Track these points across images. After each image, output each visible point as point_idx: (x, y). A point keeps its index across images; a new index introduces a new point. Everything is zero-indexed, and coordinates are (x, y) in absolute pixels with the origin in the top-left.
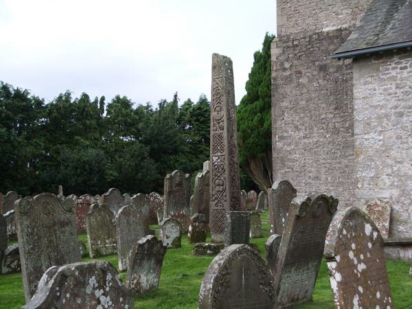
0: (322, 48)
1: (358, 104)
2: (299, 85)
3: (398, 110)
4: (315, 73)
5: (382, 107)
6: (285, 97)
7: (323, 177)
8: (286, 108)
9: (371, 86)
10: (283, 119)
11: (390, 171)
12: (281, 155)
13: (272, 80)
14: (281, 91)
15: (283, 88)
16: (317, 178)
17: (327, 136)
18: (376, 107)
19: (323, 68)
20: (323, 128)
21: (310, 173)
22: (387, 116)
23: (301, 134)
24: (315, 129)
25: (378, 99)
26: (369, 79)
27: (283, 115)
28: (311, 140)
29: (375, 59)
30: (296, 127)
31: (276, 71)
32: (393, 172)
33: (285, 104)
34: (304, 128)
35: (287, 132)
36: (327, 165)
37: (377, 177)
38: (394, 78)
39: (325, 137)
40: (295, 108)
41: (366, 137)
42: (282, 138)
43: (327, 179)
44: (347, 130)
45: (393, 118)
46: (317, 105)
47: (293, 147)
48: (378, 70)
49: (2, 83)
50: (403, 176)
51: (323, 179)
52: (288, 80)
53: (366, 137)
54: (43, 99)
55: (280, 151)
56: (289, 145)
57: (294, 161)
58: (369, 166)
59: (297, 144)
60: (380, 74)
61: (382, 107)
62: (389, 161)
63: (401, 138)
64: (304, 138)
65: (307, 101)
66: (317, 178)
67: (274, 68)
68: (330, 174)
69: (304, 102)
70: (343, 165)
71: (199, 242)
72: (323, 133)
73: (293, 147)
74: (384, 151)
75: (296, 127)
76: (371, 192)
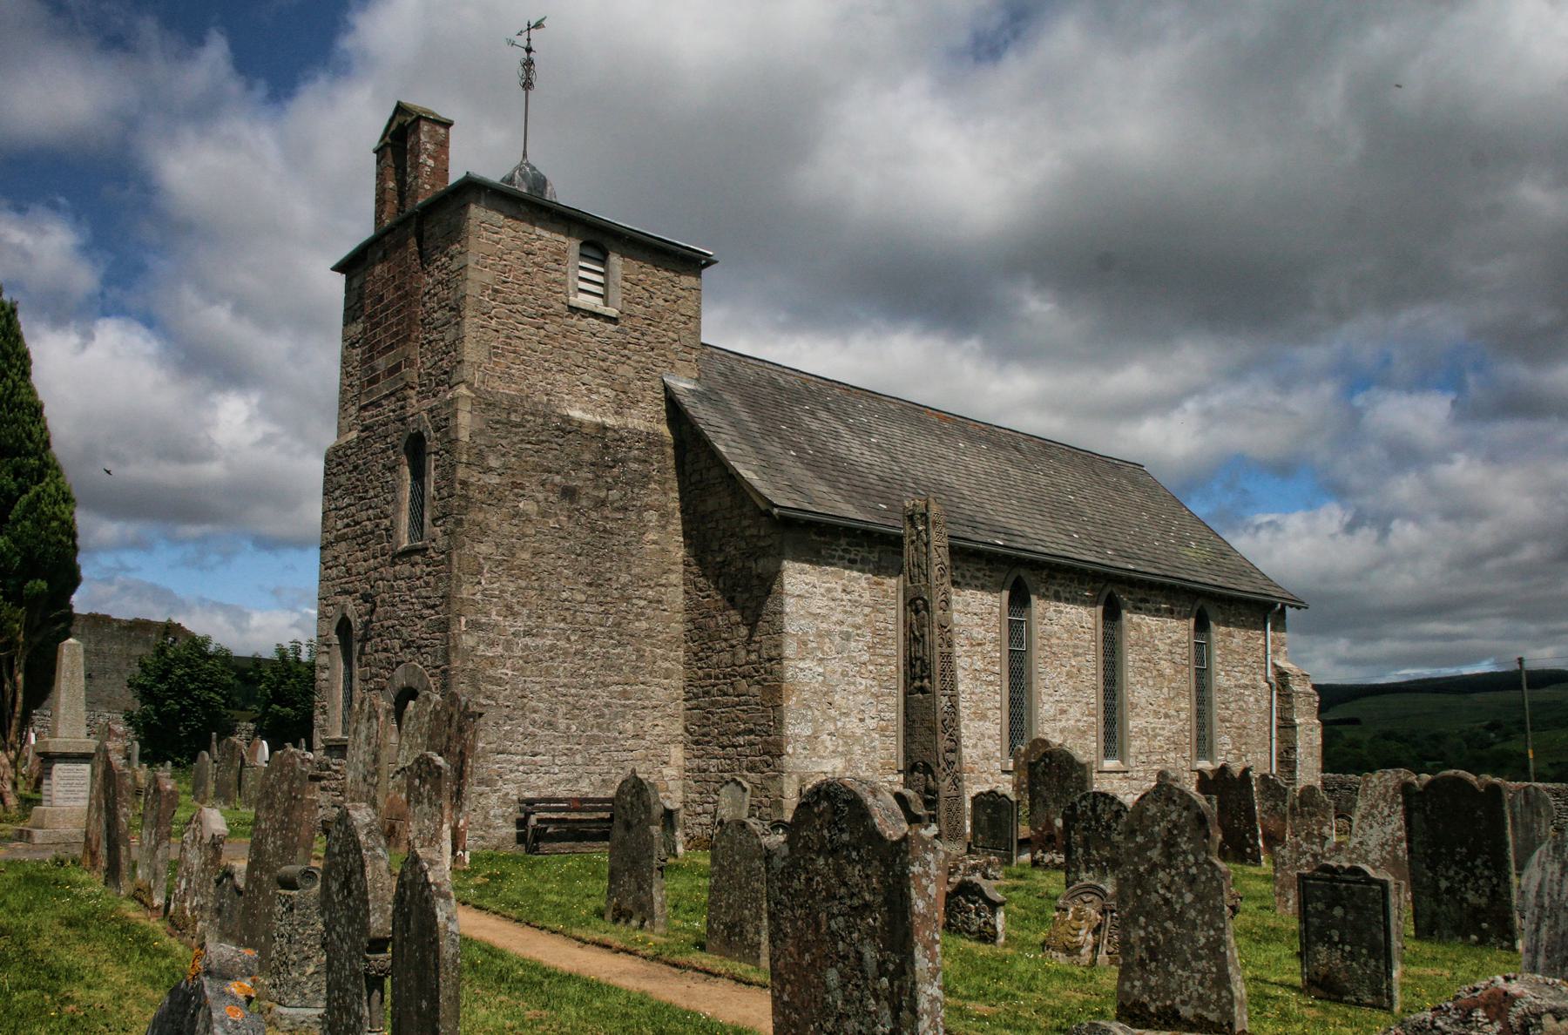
0: (568, 450)
1: (790, 605)
3: (844, 628)
5: (825, 617)
6: (484, 533)
7: (562, 723)
9: (808, 578)
11: (832, 728)
12: (470, 665)
15: (481, 509)
16: (551, 725)
17: (573, 638)
19: (569, 493)
20: (564, 620)
22: (829, 633)
23: (520, 625)
24: (550, 619)
25: (818, 604)
27: (480, 573)
28: (539, 641)
31: (468, 464)
33: (483, 548)
34: (525, 611)
35: (487, 614)
36: (570, 699)
37: (815, 737)
39: (568, 639)
40: (507, 564)
41: (801, 665)
42: (474, 626)
43: (568, 728)
45: (837, 639)
47: (500, 650)
49: (1521, 660)
51: (562, 727)
52: (495, 498)
53: (801, 665)
56: (492, 644)
57: (498, 682)
58: (804, 716)
59: (508, 646)
61: (825, 617)
62: (833, 712)
64: (527, 633)
65: (535, 554)
67: (464, 458)
69: (526, 556)
70: (599, 702)
71: (1496, 774)
73: (500, 650)
74: (826, 694)
75: (509, 608)
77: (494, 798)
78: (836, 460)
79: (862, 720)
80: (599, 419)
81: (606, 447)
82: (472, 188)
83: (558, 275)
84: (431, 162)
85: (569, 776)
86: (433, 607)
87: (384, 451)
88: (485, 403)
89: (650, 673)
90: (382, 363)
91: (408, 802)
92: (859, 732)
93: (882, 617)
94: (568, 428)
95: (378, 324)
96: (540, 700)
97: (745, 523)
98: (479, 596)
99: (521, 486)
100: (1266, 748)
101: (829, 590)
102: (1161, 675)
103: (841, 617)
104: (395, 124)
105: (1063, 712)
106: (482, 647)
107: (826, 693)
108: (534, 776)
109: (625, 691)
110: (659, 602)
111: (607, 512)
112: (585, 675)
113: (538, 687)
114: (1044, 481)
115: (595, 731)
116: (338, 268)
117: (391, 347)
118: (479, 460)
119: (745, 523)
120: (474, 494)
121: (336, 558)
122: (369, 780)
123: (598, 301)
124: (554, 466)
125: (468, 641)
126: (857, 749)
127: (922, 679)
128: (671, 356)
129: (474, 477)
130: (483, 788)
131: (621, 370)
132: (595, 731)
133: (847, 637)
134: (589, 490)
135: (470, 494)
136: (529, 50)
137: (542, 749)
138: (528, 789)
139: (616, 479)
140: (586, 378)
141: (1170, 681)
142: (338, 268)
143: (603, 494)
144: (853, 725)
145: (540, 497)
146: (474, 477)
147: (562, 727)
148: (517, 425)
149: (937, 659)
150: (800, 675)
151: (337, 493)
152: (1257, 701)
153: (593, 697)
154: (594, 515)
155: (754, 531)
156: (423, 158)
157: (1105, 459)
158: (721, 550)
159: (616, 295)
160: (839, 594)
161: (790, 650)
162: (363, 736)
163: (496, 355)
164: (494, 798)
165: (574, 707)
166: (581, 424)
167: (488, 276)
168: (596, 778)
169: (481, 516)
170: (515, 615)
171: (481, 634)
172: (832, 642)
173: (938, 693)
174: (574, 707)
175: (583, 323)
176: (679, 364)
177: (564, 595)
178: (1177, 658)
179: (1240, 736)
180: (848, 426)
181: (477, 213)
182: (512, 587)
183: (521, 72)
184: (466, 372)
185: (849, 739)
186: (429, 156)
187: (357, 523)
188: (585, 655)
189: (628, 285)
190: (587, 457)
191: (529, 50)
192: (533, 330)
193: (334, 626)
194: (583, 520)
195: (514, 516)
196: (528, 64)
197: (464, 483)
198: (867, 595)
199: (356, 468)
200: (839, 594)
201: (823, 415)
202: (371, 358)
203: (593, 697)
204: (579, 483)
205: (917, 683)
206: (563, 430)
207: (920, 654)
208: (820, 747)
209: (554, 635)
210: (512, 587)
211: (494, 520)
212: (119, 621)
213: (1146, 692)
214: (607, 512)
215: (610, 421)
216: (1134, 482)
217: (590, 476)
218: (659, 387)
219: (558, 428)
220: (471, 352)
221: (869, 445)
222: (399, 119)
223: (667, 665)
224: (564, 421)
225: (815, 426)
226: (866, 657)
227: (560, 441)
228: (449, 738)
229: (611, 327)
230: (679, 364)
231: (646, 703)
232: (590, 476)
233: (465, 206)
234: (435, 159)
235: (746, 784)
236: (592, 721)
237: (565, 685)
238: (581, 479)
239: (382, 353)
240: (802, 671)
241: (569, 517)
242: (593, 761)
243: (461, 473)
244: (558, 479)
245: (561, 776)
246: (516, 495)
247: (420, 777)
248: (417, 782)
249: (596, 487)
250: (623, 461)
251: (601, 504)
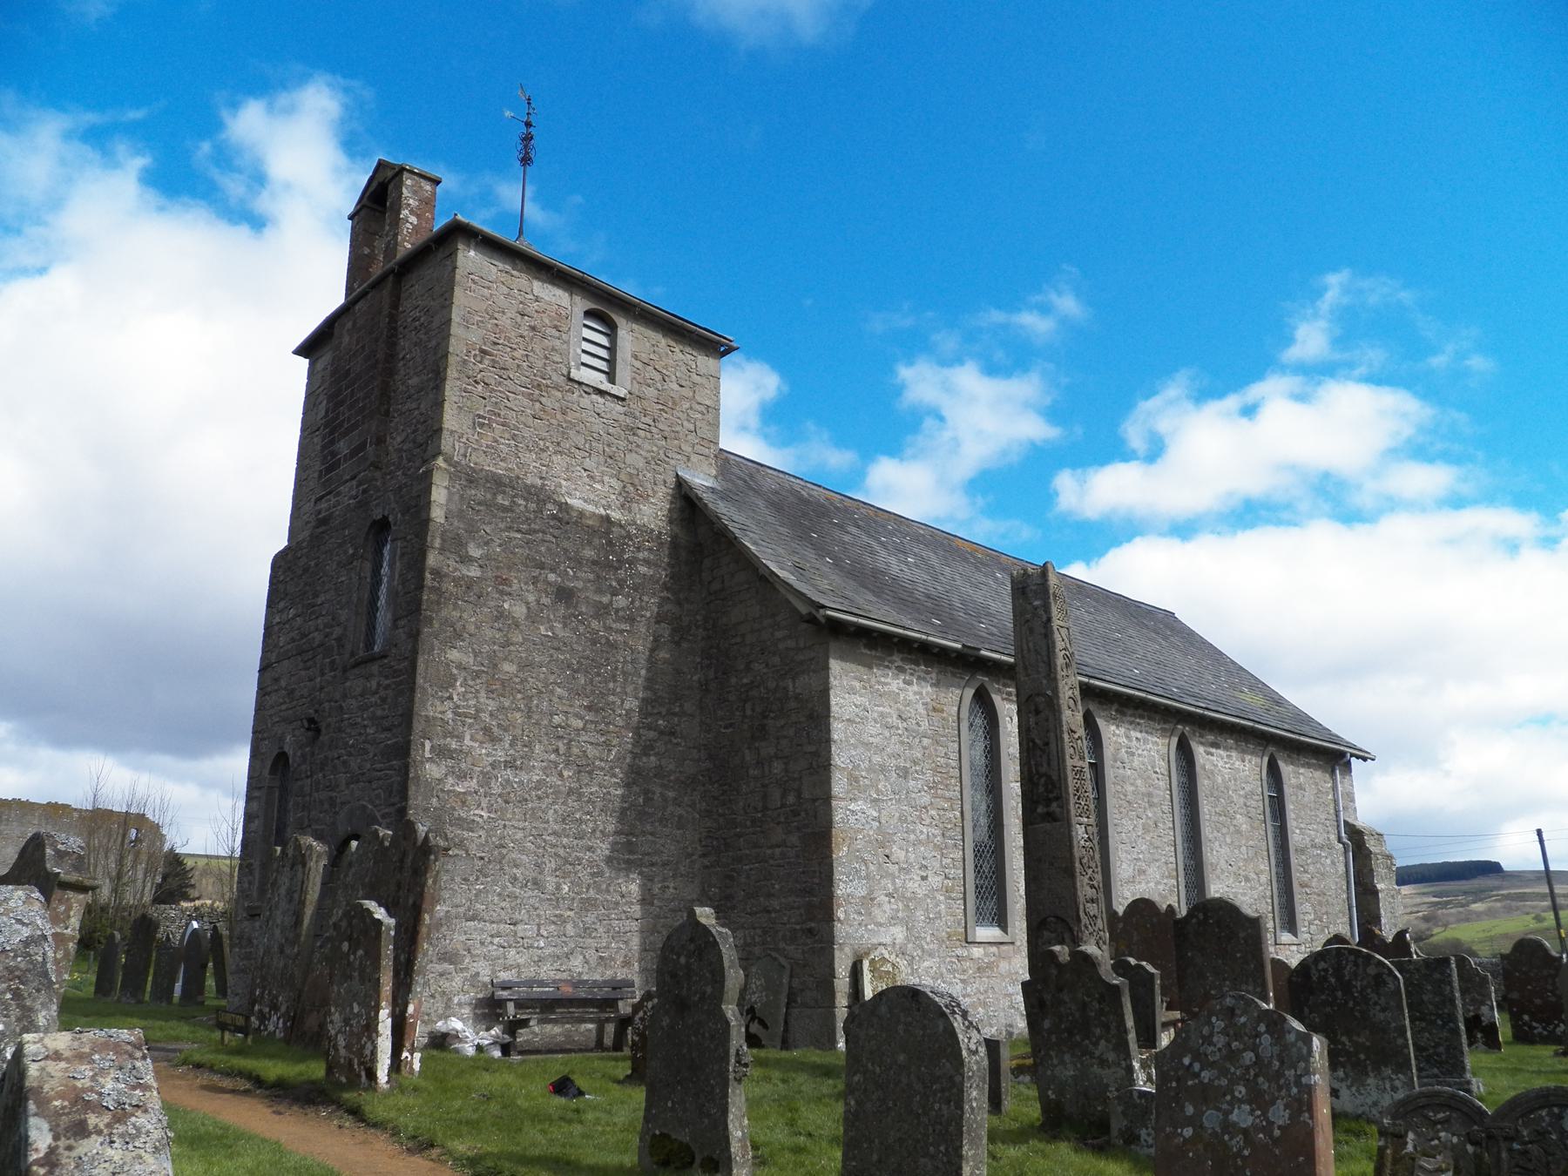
2: (501, 615)
4: (546, 600)
7: (550, 882)
8: (460, 667)
9: (858, 700)
10: (450, 698)
13: (428, 575)
14: (449, 612)
15: (456, 607)
17: (566, 773)
18: (867, 745)
19: (564, 595)
21: (516, 866)
22: (883, 769)
24: (538, 748)
26: (857, 684)
28: (524, 777)
29: (866, 646)
30: (487, 730)
32: (896, 890)
33: (454, 655)
35: (460, 738)
36: (561, 852)
37: (870, 899)
38: (894, 697)
39: (561, 775)
40: (488, 674)
42: (442, 753)
43: (558, 888)
44: (611, 768)
46: (546, 686)
48: (871, 668)
50: (910, 899)
51: (550, 887)
54: (1558, 521)
55: (434, 787)
56: (463, 776)
57: (470, 825)
59: (486, 779)
60: (873, 680)
63: (906, 821)
64: (507, 764)
66: (535, 883)
68: (565, 875)
72: (556, 764)
75: (487, 730)
76: (862, 930)
77: (457, 981)
78: (877, 574)
79: (924, 878)
80: (602, 512)
81: (610, 542)
82: (458, 232)
83: (558, 343)
84: (413, 219)
85: (558, 951)
86: (388, 729)
87: (340, 545)
88: (471, 478)
89: (661, 821)
90: (343, 447)
91: (331, 976)
92: (921, 893)
93: (942, 750)
94: (566, 518)
95: (342, 403)
96: (522, 851)
97: (779, 634)
98: (450, 715)
99: (506, 582)
100: (1346, 919)
101: (882, 715)
102: (1238, 832)
103: (898, 748)
104: (374, 184)
105: (1142, 872)
106: (450, 780)
107: (882, 842)
108: (513, 952)
109: (629, 843)
110: (673, 734)
111: (609, 622)
112: (580, 821)
113: (520, 835)
114: (1087, 617)
115: (592, 893)
116: (303, 350)
117: (355, 426)
118: (455, 545)
119: (779, 634)
120: (449, 586)
121: (276, 680)
122: (288, 951)
123: (603, 377)
124: (548, 561)
125: (433, 771)
126: (920, 915)
127: (1048, 802)
128: (687, 448)
129: (451, 565)
130: (446, 966)
131: (630, 458)
132: (592, 893)
133: (904, 773)
134: (590, 594)
135: (444, 586)
136: (528, 124)
137: (523, 915)
138: (506, 968)
139: (621, 582)
140: (588, 463)
141: (1248, 839)
142: (303, 350)
143: (605, 600)
144: (914, 885)
145: (531, 598)
146: (451, 565)
147: (550, 887)
148: (505, 509)
149: (1070, 775)
150: (852, 819)
151: (282, 605)
152: (1333, 863)
153: (590, 849)
154: (595, 624)
155: (791, 643)
156: (405, 213)
157: (1137, 605)
158: (748, 668)
159: (623, 372)
160: (894, 720)
161: (839, 785)
162: (283, 891)
163: (482, 425)
164: (457, 981)
165: (566, 862)
166: (581, 514)
167: (475, 336)
168: (592, 955)
169: (456, 614)
170: (494, 740)
171: (450, 762)
172: (887, 779)
173: (1074, 820)
174: (566, 862)
175: (586, 401)
176: (694, 458)
177: (557, 719)
178: (1253, 812)
179: (1320, 904)
180: (881, 543)
181: (469, 258)
182: (492, 705)
183: (520, 147)
184: (446, 443)
185: (909, 900)
186: (412, 212)
187: (304, 636)
188: (580, 795)
189: (638, 364)
190: (588, 553)
191: (528, 124)
192: (526, 402)
193: (269, 763)
194: (582, 629)
195: (497, 619)
196: (527, 139)
197: (437, 573)
198: (925, 725)
199: (306, 570)
200: (894, 720)
201: (854, 530)
202: (332, 442)
203: (590, 849)
204: (580, 584)
205: (1040, 810)
206: (560, 520)
207: (1043, 770)
208: (876, 911)
209: (544, 769)
210: (492, 705)
211: (471, 619)
212: (80, 811)
213: (1225, 850)
214: (609, 622)
215: (615, 515)
216: (1166, 626)
217: (591, 576)
218: (671, 480)
219: (554, 517)
220: (451, 419)
221: (907, 564)
222: (380, 178)
223: (680, 811)
224: (560, 510)
225: (847, 538)
226: (926, 799)
227: (556, 532)
228: (399, 886)
229: (619, 408)
230: (694, 458)
231: (655, 859)
232: (591, 576)
233: (452, 255)
234: (418, 216)
235: (782, 960)
236: (587, 880)
237: (554, 833)
238: (580, 580)
239: (345, 434)
240: (852, 812)
241: (565, 625)
242: (587, 931)
243: (432, 559)
244: (552, 577)
245: (547, 952)
246: (502, 593)
247: (350, 939)
248: (345, 946)
249: (599, 591)
250: (632, 562)
251: (602, 611)
